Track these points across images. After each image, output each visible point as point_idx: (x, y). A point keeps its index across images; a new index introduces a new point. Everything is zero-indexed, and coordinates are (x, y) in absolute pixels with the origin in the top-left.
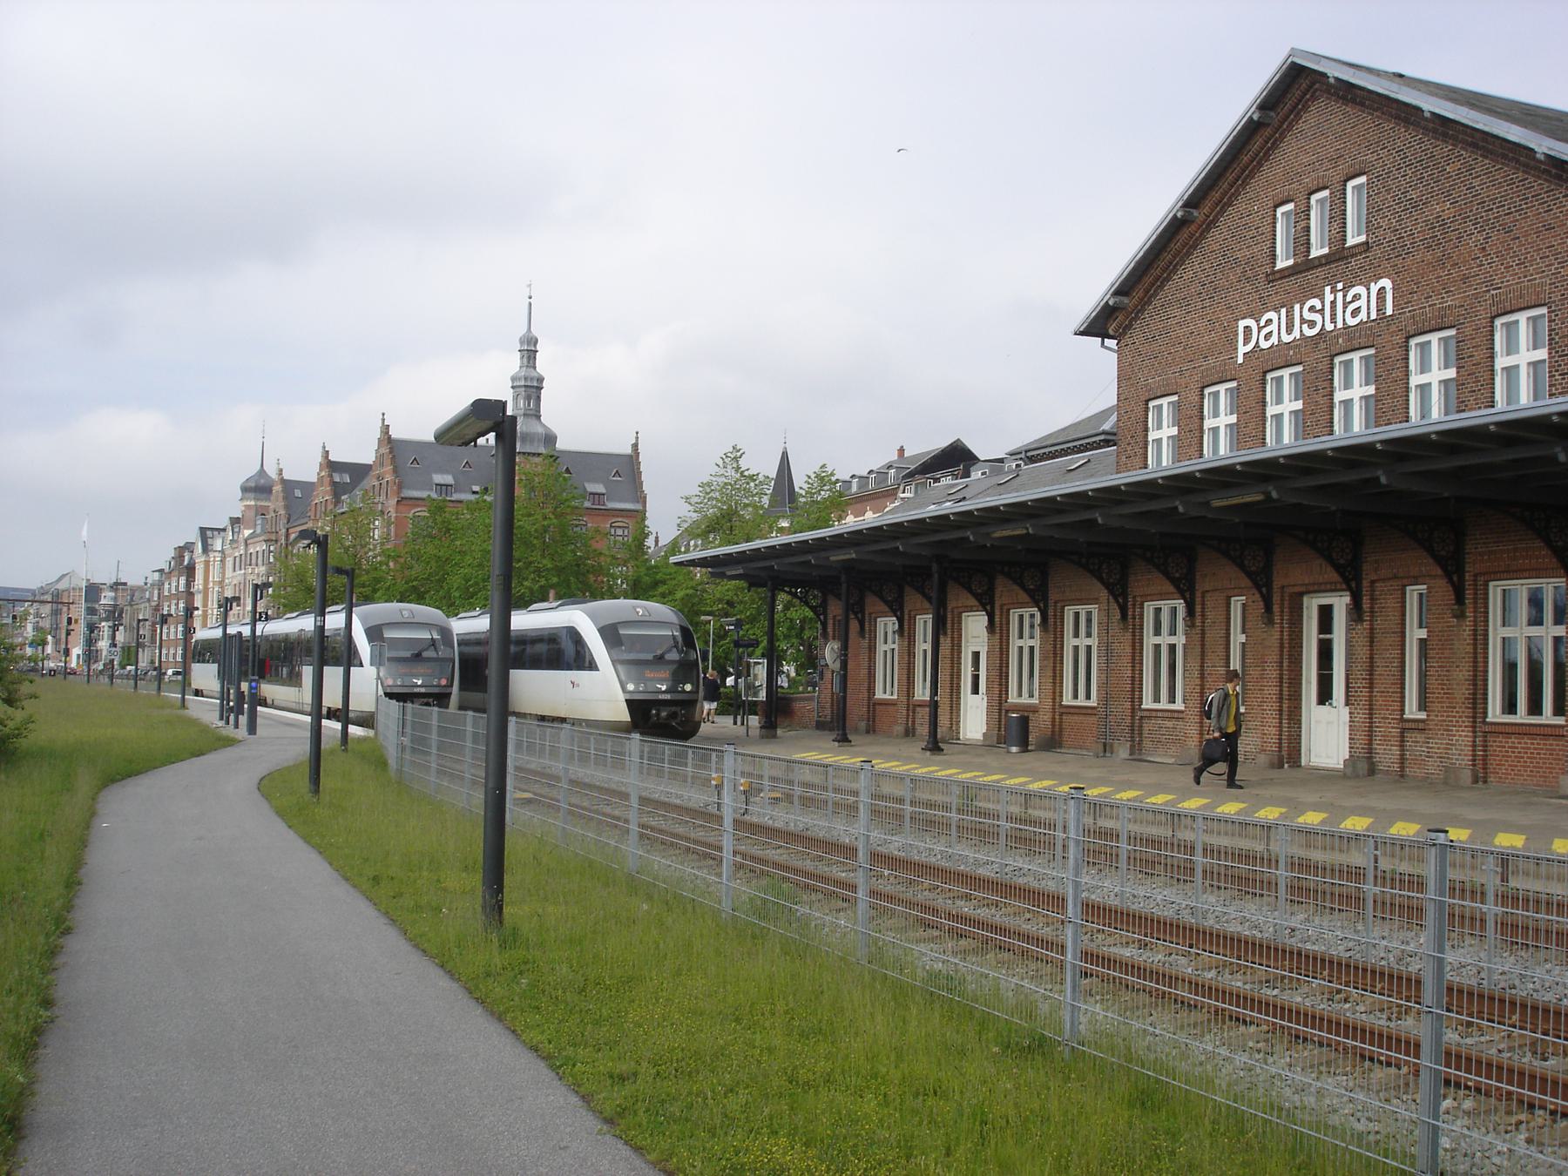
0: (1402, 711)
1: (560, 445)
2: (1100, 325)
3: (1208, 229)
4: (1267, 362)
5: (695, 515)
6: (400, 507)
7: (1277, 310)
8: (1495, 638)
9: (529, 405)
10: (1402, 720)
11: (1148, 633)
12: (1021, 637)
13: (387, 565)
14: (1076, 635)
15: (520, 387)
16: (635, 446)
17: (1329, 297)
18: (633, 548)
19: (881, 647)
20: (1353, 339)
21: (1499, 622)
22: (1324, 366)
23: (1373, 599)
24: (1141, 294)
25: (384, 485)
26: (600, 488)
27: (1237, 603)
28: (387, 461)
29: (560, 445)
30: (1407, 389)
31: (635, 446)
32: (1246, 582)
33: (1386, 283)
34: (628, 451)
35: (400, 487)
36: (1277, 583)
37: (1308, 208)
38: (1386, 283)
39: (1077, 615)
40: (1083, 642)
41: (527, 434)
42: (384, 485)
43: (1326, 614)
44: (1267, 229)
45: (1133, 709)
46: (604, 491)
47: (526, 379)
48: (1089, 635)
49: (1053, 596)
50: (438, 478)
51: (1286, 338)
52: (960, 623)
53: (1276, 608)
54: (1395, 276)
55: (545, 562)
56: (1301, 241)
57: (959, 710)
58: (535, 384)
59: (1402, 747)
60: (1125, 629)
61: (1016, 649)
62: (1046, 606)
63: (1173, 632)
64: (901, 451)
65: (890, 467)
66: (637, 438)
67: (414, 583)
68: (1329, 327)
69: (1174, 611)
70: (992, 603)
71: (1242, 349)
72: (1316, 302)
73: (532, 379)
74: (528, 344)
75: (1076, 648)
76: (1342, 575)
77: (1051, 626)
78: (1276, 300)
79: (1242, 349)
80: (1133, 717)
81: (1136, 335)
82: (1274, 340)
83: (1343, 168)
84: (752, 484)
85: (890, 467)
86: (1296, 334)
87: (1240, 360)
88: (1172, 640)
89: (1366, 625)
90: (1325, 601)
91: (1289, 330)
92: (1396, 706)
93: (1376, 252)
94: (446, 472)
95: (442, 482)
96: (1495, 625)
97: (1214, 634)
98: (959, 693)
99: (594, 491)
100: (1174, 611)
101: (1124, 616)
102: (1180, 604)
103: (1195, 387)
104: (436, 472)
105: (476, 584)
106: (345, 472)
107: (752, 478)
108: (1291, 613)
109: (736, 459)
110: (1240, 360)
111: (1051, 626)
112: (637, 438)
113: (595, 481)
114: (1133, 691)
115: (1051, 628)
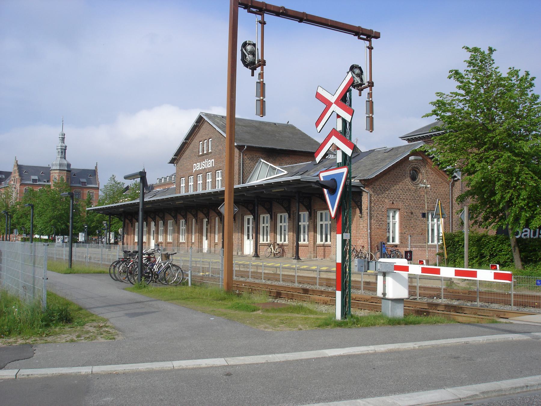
0: (215, 241)
1: (72, 167)
2: (172, 161)
3: (190, 144)
4: (198, 173)
5: (103, 194)
6: (21, 187)
7: (199, 163)
8: (318, 225)
9: (62, 155)
10: (215, 243)
11: (318, 221)
12: (264, 223)
13: (17, 206)
14: (264, 223)
15: (59, 149)
16: (96, 167)
17: (206, 162)
18: (87, 203)
19: (181, 228)
20: (209, 170)
21: (320, 220)
22: (205, 175)
23: (211, 220)
24: (179, 156)
25: (16, 180)
26: (84, 180)
27: (217, 218)
28: (17, 171)
29: (72, 167)
30: (216, 181)
31: (96, 167)
32: (172, 218)
33: (213, 160)
34: (94, 168)
35: (21, 180)
36: (199, 216)
37: (204, 143)
38: (213, 160)
39: (264, 217)
40: (265, 225)
41: (61, 164)
42: (16, 180)
43: (249, 219)
44: (198, 146)
45: (178, 242)
46: (86, 181)
47: (61, 146)
48: (267, 223)
49: (166, 218)
50: (33, 177)
51: (200, 169)
52: (150, 224)
53: (198, 222)
54: (215, 159)
55: (61, 207)
56: (203, 151)
57: (150, 242)
58: (64, 148)
59: (215, 248)
60: (176, 225)
61: (262, 227)
62: (164, 220)
63: (267, 223)
64: (480, 49)
65: (173, 175)
66: (97, 165)
67: (25, 212)
68: (206, 167)
69: (267, 217)
70: (155, 220)
71: (194, 170)
72: (204, 162)
73: (63, 147)
74: (62, 135)
75: (281, 226)
76: (205, 215)
77: (274, 219)
78: (199, 161)
79: (194, 170)
80: (178, 244)
81: (179, 164)
82: (198, 169)
83: (209, 137)
84: (119, 185)
85: (173, 175)
86: (201, 168)
87: (194, 172)
88: (326, 223)
89: (210, 225)
90: (248, 218)
91: (201, 167)
92: (214, 240)
93: (212, 154)
94: (35, 175)
95: (34, 179)
96: (318, 221)
97: (190, 226)
98: (150, 240)
99: (83, 181)
100: (267, 217)
101: (176, 223)
102: (269, 215)
103: (187, 176)
104: (33, 175)
105: (42, 213)
106: (3, 174)
107: (119, 183)
108: (201, 222)
109: (114, 179)
110: (194, 172)
111: (274, 219)
112: (97, 165)
113: (83, 178)
114: (178, 238)
115: (273, 220)
